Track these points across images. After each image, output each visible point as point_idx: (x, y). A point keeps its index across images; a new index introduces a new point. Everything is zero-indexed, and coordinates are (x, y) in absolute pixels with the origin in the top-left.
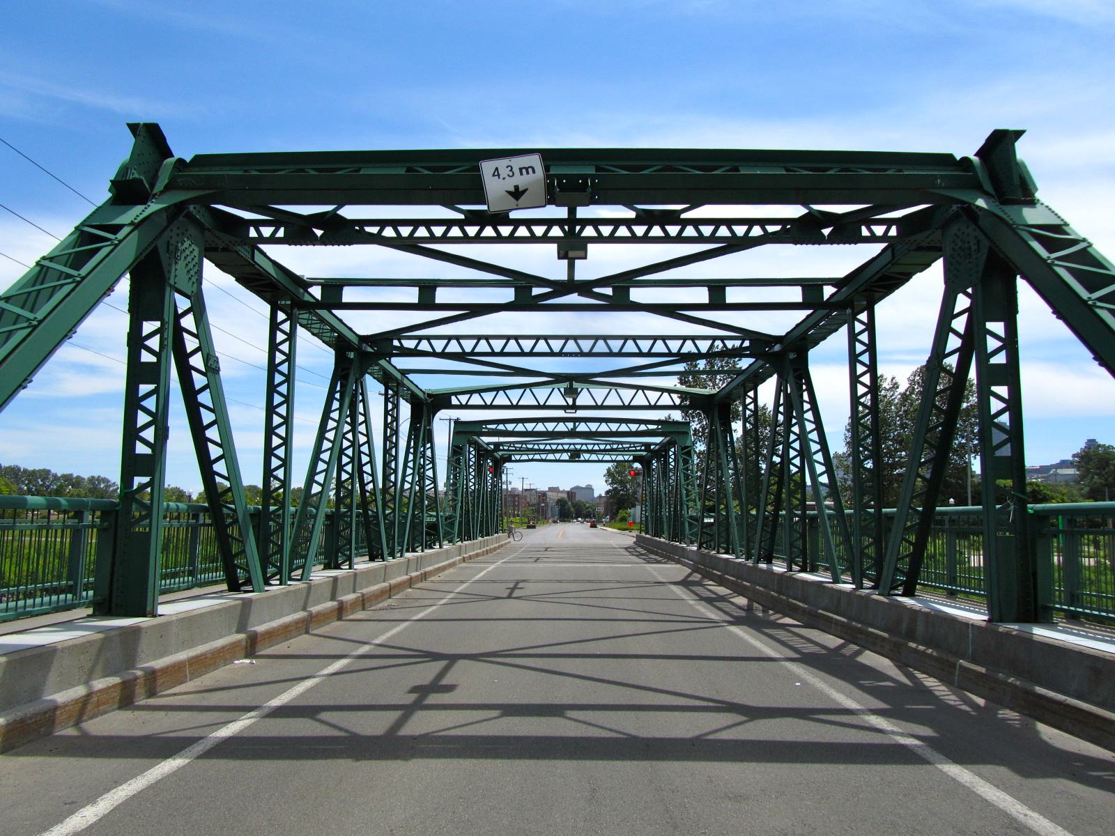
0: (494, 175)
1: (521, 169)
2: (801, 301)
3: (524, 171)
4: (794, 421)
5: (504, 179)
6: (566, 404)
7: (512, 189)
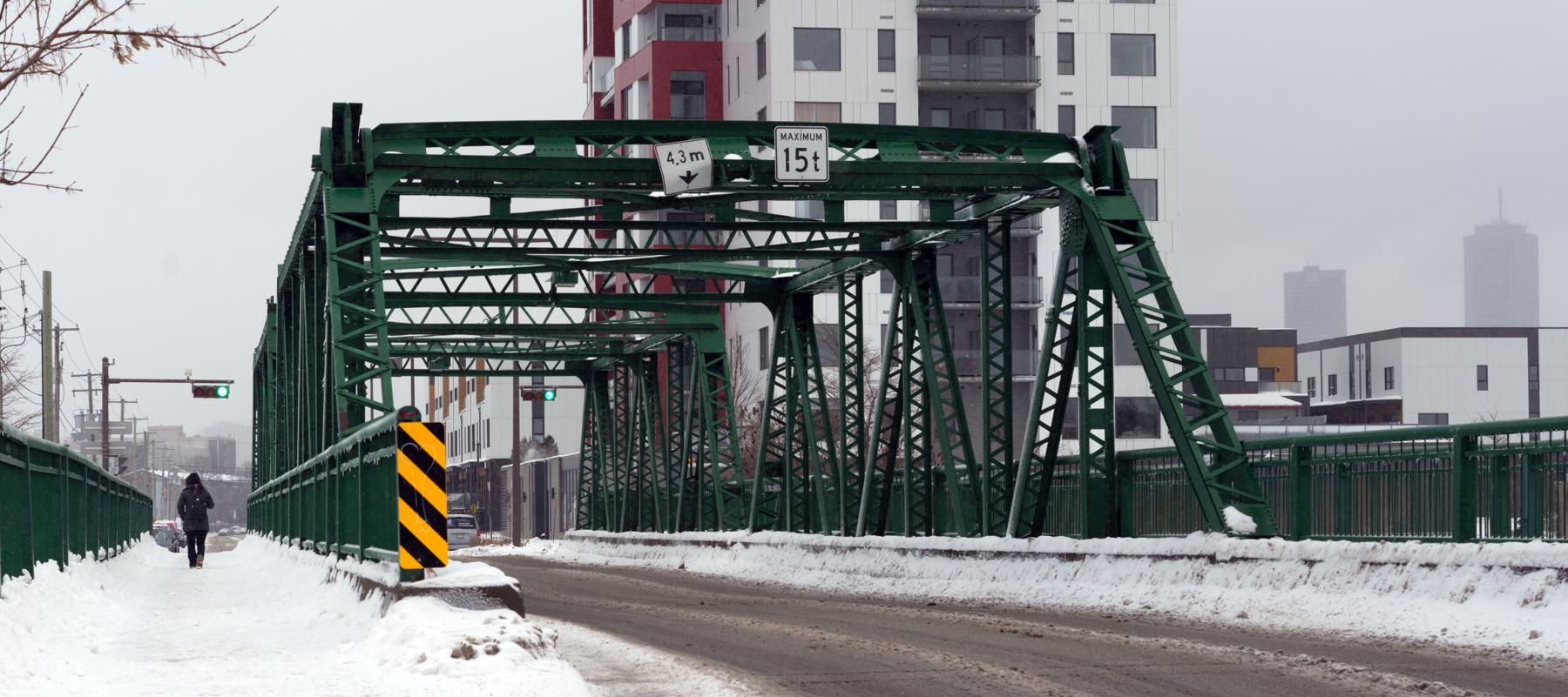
0: (668, 161)
1: (691, 155)
2: (488, 213)
3: (694, 156)
4: (916, 344)
5: (677, 164)
6: (400, 290)
7: (685, 175)
